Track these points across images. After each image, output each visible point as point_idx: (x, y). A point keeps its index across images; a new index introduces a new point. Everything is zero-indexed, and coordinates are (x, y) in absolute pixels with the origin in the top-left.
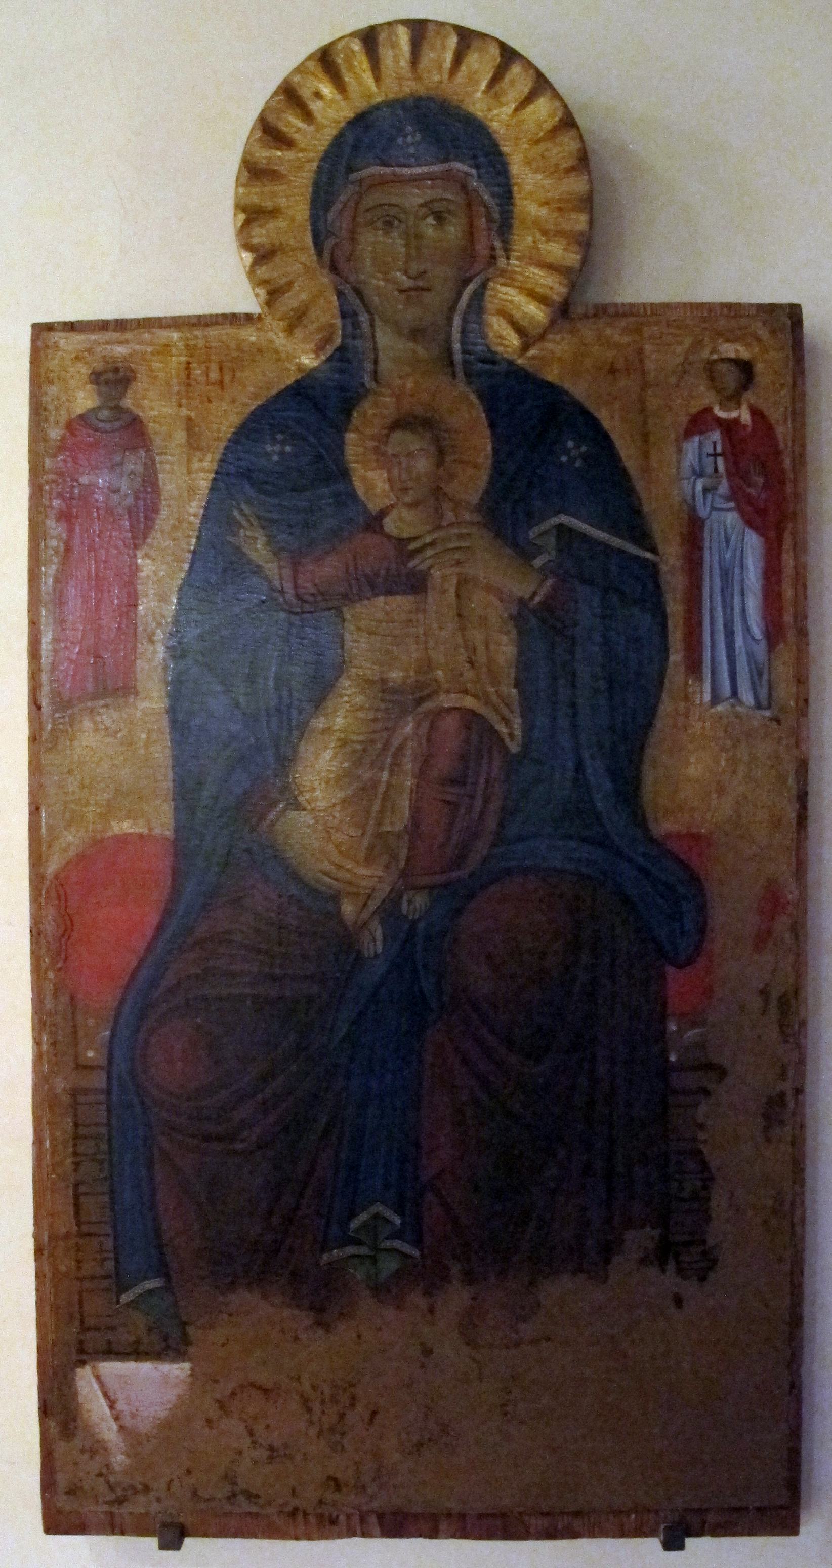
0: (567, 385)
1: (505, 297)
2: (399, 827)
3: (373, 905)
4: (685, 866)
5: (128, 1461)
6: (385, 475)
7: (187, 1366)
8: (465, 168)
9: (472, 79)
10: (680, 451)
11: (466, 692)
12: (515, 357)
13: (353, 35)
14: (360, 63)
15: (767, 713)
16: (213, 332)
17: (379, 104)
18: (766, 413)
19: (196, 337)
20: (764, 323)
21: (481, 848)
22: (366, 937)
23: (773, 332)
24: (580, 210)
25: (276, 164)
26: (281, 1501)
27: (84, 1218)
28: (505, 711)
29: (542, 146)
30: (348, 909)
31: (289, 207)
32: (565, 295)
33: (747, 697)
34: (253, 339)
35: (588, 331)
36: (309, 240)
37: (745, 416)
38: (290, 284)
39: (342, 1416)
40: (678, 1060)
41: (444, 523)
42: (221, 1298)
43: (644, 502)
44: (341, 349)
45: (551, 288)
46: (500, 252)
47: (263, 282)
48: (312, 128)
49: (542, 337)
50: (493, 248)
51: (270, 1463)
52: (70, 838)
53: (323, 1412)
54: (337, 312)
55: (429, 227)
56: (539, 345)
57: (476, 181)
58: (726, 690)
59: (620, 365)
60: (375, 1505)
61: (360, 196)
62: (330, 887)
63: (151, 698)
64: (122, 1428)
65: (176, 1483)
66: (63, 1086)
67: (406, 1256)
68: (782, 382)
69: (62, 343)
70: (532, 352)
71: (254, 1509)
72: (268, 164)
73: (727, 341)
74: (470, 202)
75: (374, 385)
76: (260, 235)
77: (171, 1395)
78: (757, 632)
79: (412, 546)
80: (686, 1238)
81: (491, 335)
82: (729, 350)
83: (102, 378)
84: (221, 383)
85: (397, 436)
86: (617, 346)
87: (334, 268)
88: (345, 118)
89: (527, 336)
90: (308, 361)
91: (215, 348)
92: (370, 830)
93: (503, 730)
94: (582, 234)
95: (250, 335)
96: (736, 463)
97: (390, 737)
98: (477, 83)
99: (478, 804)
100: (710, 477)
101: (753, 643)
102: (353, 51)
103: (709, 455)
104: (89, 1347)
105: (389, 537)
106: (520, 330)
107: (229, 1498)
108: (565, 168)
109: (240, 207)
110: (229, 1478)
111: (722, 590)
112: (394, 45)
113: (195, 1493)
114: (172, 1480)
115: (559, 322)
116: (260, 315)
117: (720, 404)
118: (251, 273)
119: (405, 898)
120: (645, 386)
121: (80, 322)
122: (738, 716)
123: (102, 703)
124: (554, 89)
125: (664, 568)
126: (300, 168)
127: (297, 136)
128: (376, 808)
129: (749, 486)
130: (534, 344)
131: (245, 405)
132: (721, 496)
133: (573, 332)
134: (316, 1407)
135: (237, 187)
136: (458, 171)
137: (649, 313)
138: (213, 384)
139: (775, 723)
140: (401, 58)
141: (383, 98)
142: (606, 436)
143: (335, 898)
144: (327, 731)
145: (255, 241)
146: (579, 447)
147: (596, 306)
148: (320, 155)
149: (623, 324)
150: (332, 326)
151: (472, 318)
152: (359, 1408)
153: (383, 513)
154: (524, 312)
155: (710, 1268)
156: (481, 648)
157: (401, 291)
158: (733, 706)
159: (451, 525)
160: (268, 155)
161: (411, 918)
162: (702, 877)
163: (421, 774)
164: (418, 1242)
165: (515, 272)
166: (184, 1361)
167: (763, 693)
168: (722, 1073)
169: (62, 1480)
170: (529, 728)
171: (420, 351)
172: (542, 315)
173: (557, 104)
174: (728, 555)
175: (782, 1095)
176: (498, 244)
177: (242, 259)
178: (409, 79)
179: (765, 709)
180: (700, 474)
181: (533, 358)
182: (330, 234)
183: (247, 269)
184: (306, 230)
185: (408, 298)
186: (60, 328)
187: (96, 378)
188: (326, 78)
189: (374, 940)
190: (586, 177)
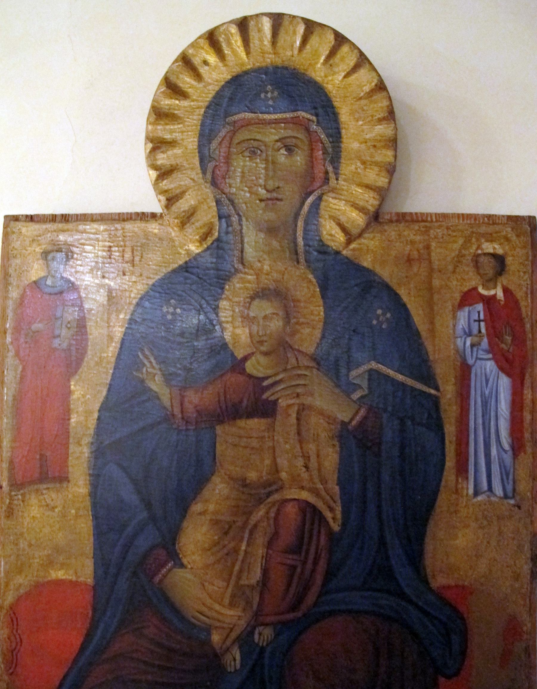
0: (378, 270)
1: (334, 207)
2: (253, 581)
3: (234, 635)
4: (455, 610)
8: (309, 116)
9: (316, 54)
10: (454, 317)
11: (302, 488)
12: (341, 249)
13: (231, 22)
14: (236, 41)
15: (512, 502)
16: (128, 226)
17: (249, 70)
18: (514, 292)
19: (116, 229)
20: (513, 229)
21: (311, 598)
22: (228, 658)
23: (518, 236)
24: (386, 147)
25: (175, 109)
28: (332, 503)
29: (363, 102)
30: (216, 638)
31: (182, 140)
32: (377, 207)
33: (498, 490)
34: (156, 231)
35: (392, 231)
36: (197, 163)
37: (500, 294)
38: (183, 193)
41: (289, 367)
43: (431, 353)
44: (218, 240)
45: (367, 201)
46: (332, 175)
47: (164, 192)
48: (201, 85)
49: (360, 235)
50: (327, 173)
52: (21, 581)
54: (215, 214)
55: (282, 157)
56: (358, 241)
57: (316, 125)
58: (485, 485)
59: (415, 254)
61: (234, 132)
62: (205, 623)
63: (79, 487)
68: (525, 270)
69: (24, 230)
70: (352, 246)
72: (170, 109)
73: (487, 241)
75: (241, 267)
76: (162, 159)
78: (507, 446)
79: (265, 383)
81: (325, 233)
82: (489, 247)
84: (132, 262)
85: (256, 302)
86: (412, 242)
87: (214, 183)
88: (224, 79)
89: (350, 235)
90: (194, 248)
91: (129, 236)
92: (232, 582)
93: (328, 515)
94: (390, 163)
95: (154, 227)
97: (248, 519)
98: (319, 57)
99: (309, 566)
100: (476, 336)
101: (503, 453)
102: (232, 34)
103: (475, 321)
105: (250, 376)
106: (344, 229)
108: (379, 119)
109: (149, 139)
111: (483, 416)
112: (260, 31)
115: (372, 224)
116: (161, 214)
117: (483, 285)
118: (156, 184)
119: (257, 632)
120: (431, 270)
121: (38, 216)
122: (491, 503)
123: (45, 486)
124: (370, 63)
125: (443, 401)
126: (192, 113)
127: (189, 90)
128: (237, 568)
129: (502, 342)
130: (355, 240)
132: (483, 350)
133: (382, 232)
135: (147, 124)
136: (303, 117)
137: (434, 220)
138: (127, 262)
139: (517, 508)
140: (264, 39)
141: (252, 66)
142: (404, 305)
143: (208, 630)
144: (203, 513)
145: (159, 163)
147: (398, 214)
148: (206, 104)
149: (417, 228)
150: (212, 223)
154: (348, 217)
157: (261, 200)
158: (489, 497)
159: (293, 368)
160: (169, 103)
161: (261, 644)
162: (465, 616)
163: (270, 545)
165: (343, 190)
167: (509, 488)
170: (346, 513)
171: (275, 244)
172: (361, 220)
173: (374, 74)
174: (487, 392)
176: (330, 169)
177: (149, 175)
178: (270, 53)
179: (511, 498)
180: (470, 334)
181: (354, 250)
182: (211, 158)
183: (153, 182)
184: (196, 156)
185: (266, 205)
186: (24, 219)
188: (211, 51)
189: (235, 660)
190: (393, 125)
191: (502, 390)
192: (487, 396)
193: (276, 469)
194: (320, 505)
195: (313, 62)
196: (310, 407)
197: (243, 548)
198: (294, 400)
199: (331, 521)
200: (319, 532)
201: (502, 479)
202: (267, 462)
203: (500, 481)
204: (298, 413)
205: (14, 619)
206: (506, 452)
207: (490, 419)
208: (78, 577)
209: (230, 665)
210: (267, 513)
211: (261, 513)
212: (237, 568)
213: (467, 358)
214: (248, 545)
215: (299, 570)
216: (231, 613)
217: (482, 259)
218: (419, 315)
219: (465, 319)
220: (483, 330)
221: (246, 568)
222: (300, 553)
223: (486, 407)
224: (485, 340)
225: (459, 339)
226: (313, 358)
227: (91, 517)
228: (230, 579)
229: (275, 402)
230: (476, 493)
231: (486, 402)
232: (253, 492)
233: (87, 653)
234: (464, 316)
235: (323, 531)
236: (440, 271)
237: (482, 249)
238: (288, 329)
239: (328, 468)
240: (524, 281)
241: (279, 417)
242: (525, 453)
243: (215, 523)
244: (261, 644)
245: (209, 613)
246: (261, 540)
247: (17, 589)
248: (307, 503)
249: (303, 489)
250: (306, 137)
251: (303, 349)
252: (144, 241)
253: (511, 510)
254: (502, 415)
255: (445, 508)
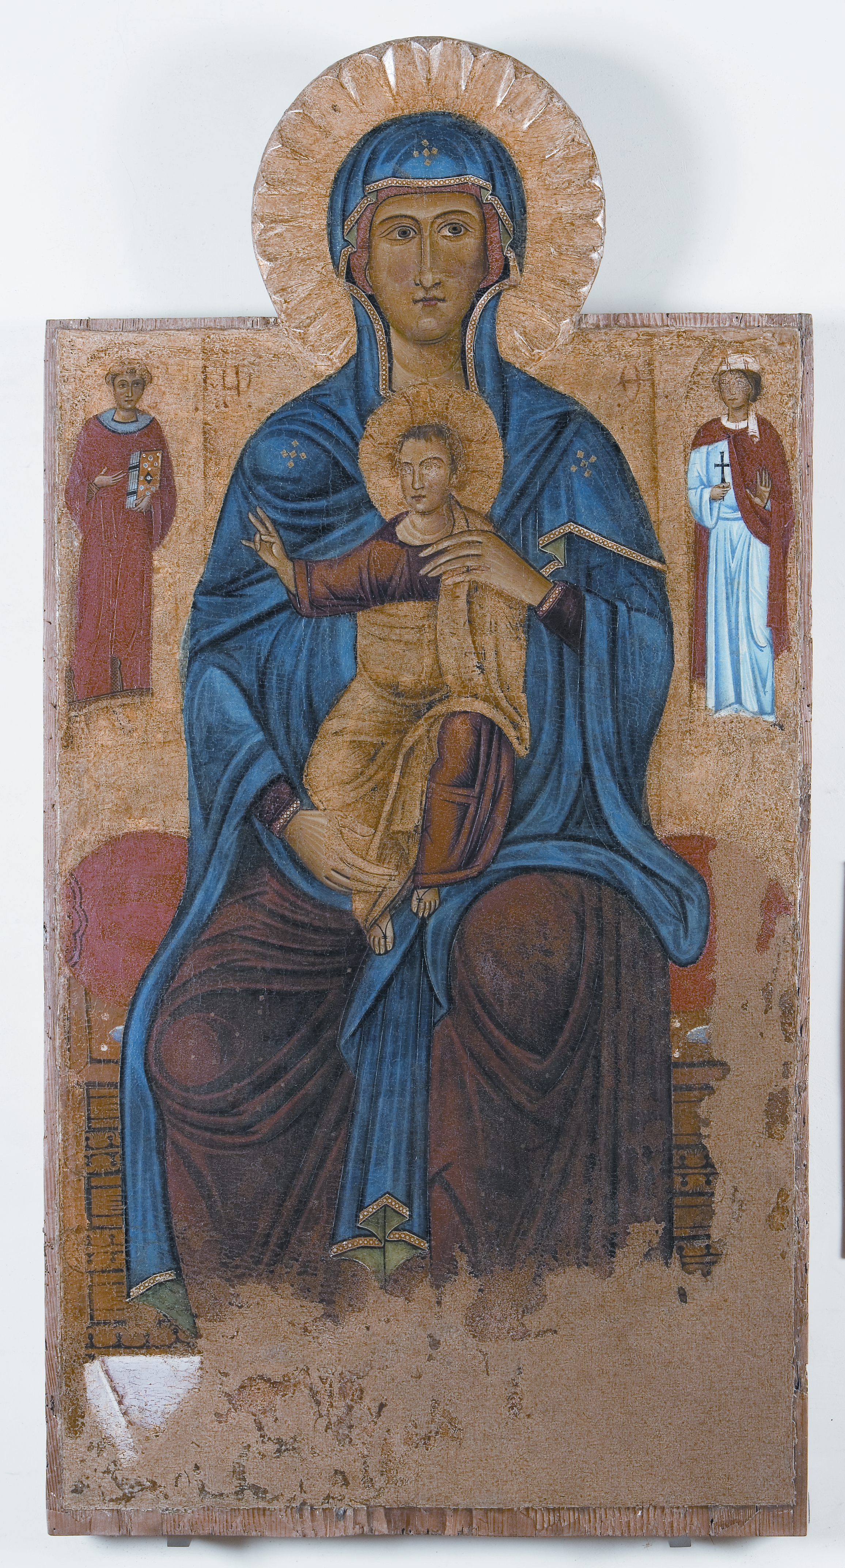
0: (578, 396)
2: (410, 827)
3: (383, 902)
5: (136, 1457)
6: (399, 482)
7: (197, 1359)
10: (686, 461)
26: (288, 1496)
27: (95, 1212)
33: (751, 703)
37: (753, 427)
39: (350, 1408)
40: (683, 1055)
42: (232, 1290)
51: (278, 1457)
52: (86, 835)
53: (331, 1406)
58: (731, 696)
59: (631, 374)
60: (381, 1501)
61: (377, 205)
64: (130, 1423)
65: (184, 1479)
66: (76, 1080)
67: (415, 1247)
71: (262, 1505)
74: (486, 218)
77: (182, 1388)
78: (762, 642)
80: (689, 1232)
82: (737, 362)
83: (118, 379)
85: (410, 443)
87: (350, 278)
92: (381, 827)
93: (511, 734)
96: (743, 474)
97: (401, 740)
100: (718, 486)
104: (98, 1341)
105: (403, 544)
107: (237, 1493)
110: (239, 1473)
113: (202, 1489)
114: (179, 1476)
116: (276, 319)
123: (119, 701)
125: (669, 577)
128: (387, 808)
131: (262, 410)
132: (727, 506)
134: (325, 1400)
138: (230, 389)
143: (348, 894)
146: (589, 457)
151: (488, 314)
152: (367, 1401)
153: (396, 520)
155: (714, 1263)
156: (491, 656)
163: (433, 773)
164: (426, 1234)
166: (193, 1354)
168: (723, 1066)
169: (69, 1479)
175: (785, 1090)
176: (511, 255)
179: (769, 714)
180: (709, 484)
187: (112, 378)
189: (385, 937)
191: (755, 562)
192: (733, 570)
193: (438, 671)
194: (499, 719)
195: (486, 105)
196: (485, 587)
197: (396, 780)
198: (463, 576)
199: (515, 741)
200: (499, 756)
201: (756, 686)
202: (428, 661)
203: (753, 689)
204: (468, 595)
205: (77, 890)
206: (760, 648)
207: (738, 603)
208: (167, 827)
209: (379, 942)
210: (428, 731)
211: (421, 731)
212: (387, 808)
213: (705, 518)
214: (403, 775)
215: (472, 809)
216: (380, 870)
217: (727, 378)
218: (636, 458)
219: (701, 463)
220: (729, 479)
221: (400, 807)
222: (474, 787)
223: (732, 584)
224: (731, 494)
225: (693, 491)
226: (489, 518)
227: (185, 743)
228: (378, 823)
229: (437, 579)
230: (718, 707)
231: (732, 580)
232: (408, 702)
233: (181, 931)
234: (701, 458)
235: (504, 757)
236: (667, 397)
237: (728, 364)
238: (454, 480)
239: (511, 669)
240: (789, 408)
241: (443, 601)
242: (789, 651)
243: (356, 745)
244: (421, 915)
245: (348, 870)
246: (420, 768)
247: (81, 848)
248: (483, 716)
249: (477, 698)
250: (478, 212)
251: (475, 507)
252: (253, 359)
253: (769, 730)
254: (755, 597)
255: (675, 727)
